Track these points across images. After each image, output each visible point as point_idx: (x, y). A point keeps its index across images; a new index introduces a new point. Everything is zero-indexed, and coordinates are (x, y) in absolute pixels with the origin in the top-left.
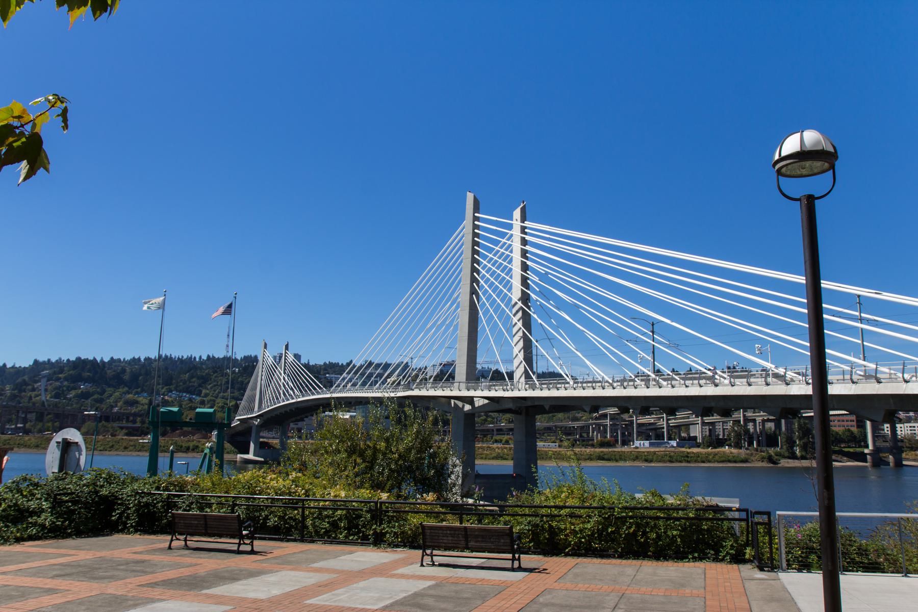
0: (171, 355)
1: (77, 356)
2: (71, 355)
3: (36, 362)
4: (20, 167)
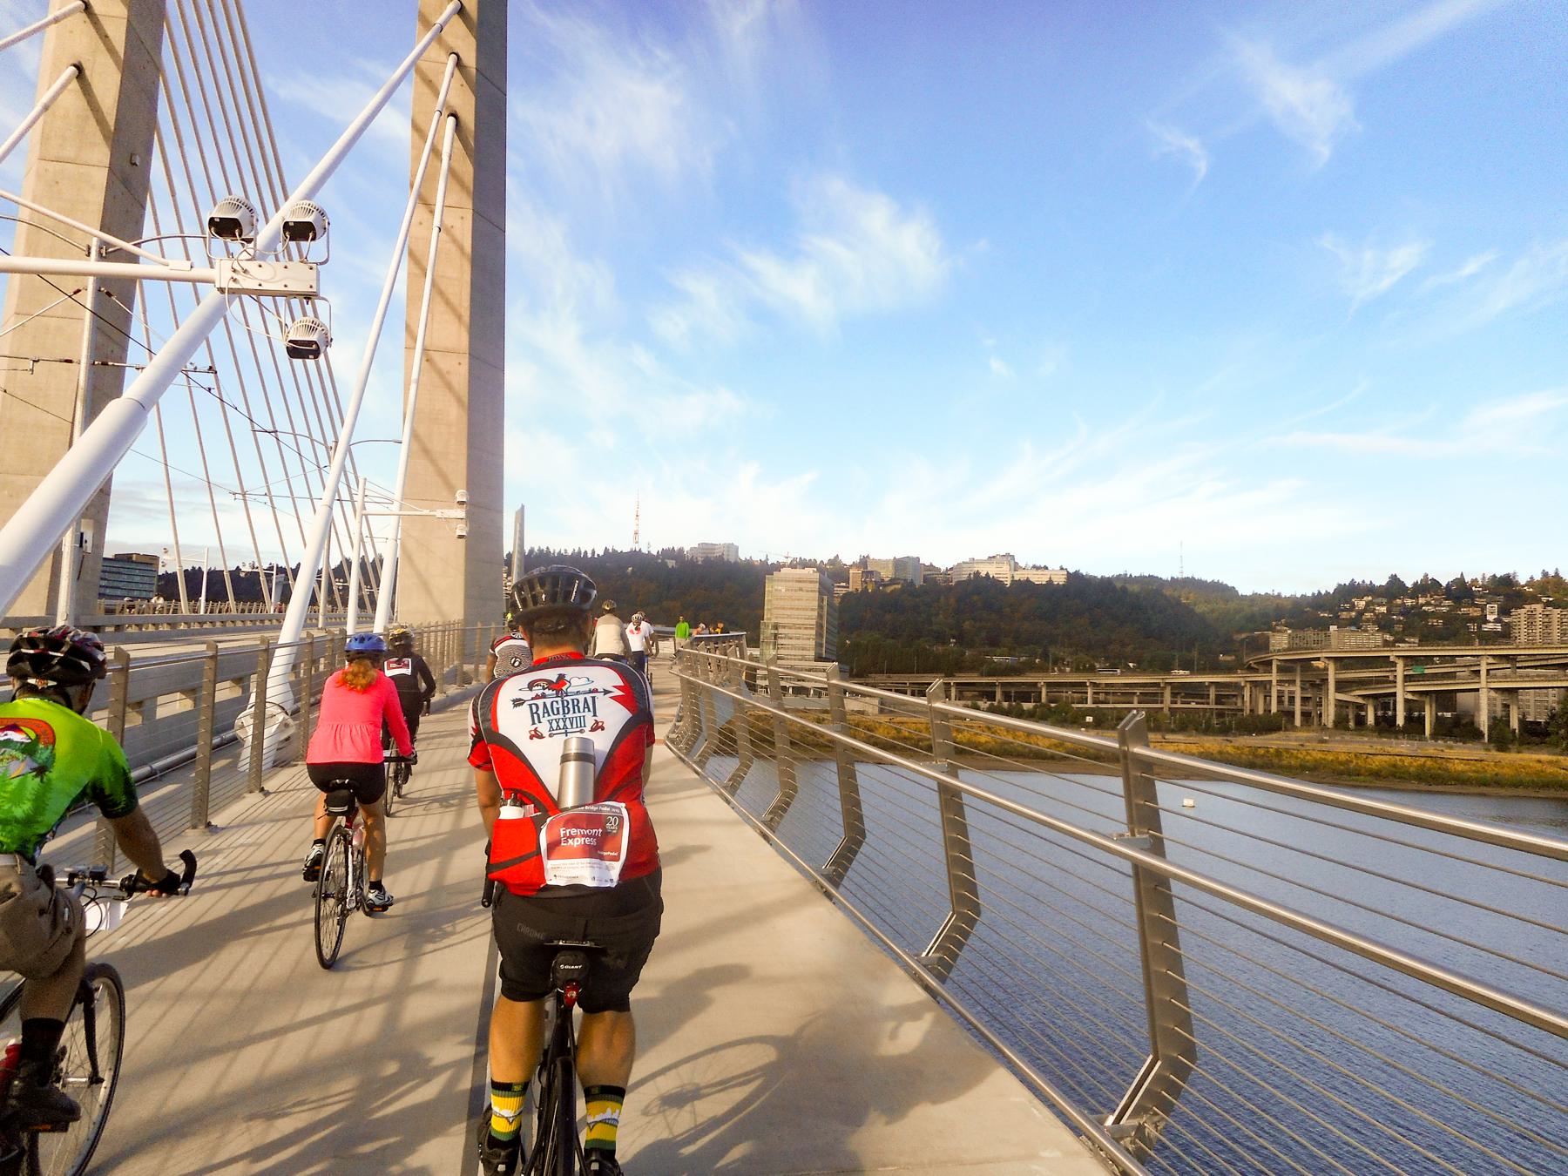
0: (548, 548)
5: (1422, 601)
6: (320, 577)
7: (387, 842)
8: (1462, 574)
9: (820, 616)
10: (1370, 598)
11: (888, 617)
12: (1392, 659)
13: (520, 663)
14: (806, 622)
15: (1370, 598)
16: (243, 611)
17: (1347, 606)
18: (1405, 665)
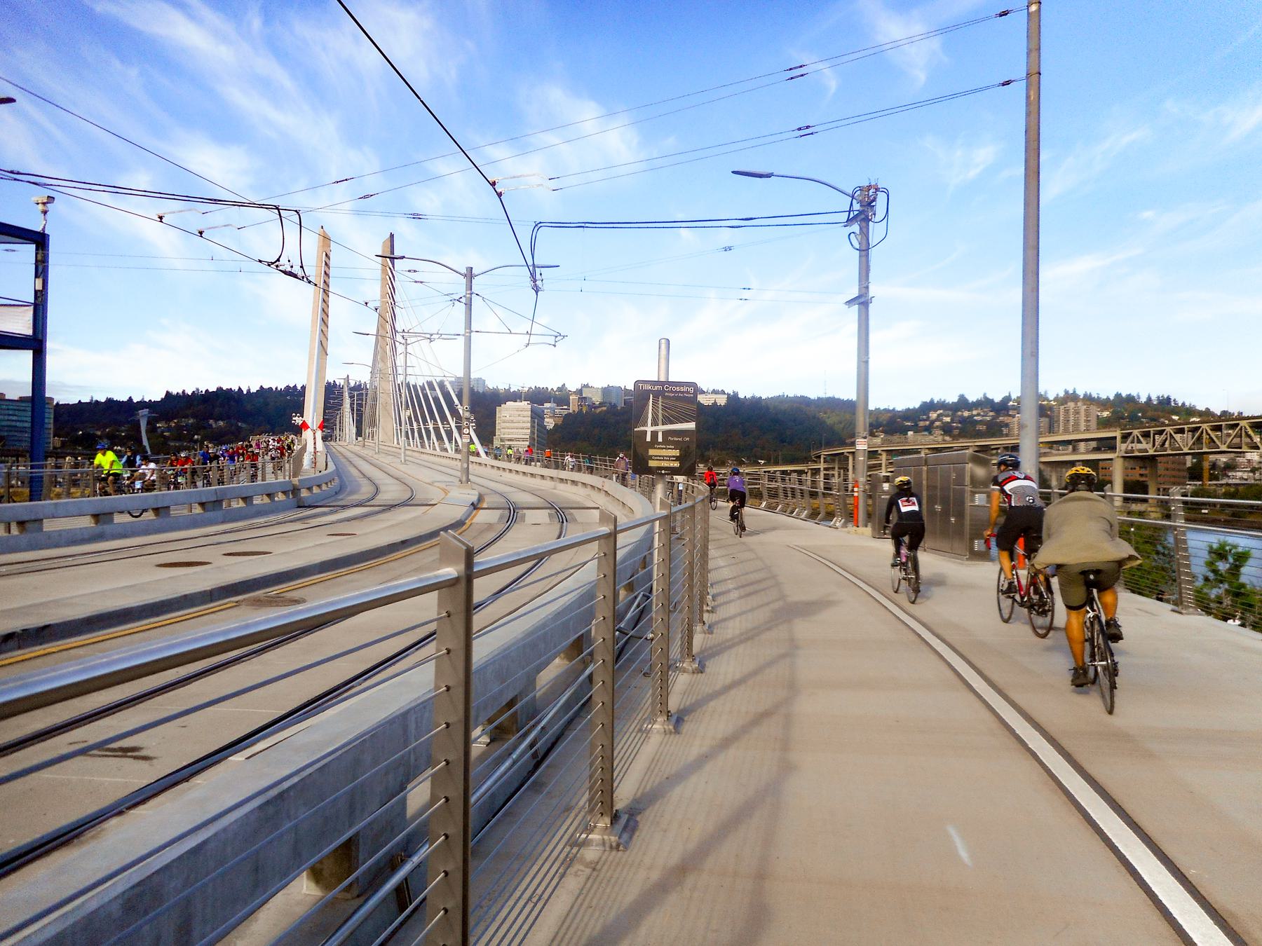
1: (959, 395)
2: (209, 384)
3: (168, 394)
9: (532, 433)
10: (941, 411)
11: (596, 431)
12: (879, 452)
14: (524, 437)
15: (941, 411)
17: (925, 417)
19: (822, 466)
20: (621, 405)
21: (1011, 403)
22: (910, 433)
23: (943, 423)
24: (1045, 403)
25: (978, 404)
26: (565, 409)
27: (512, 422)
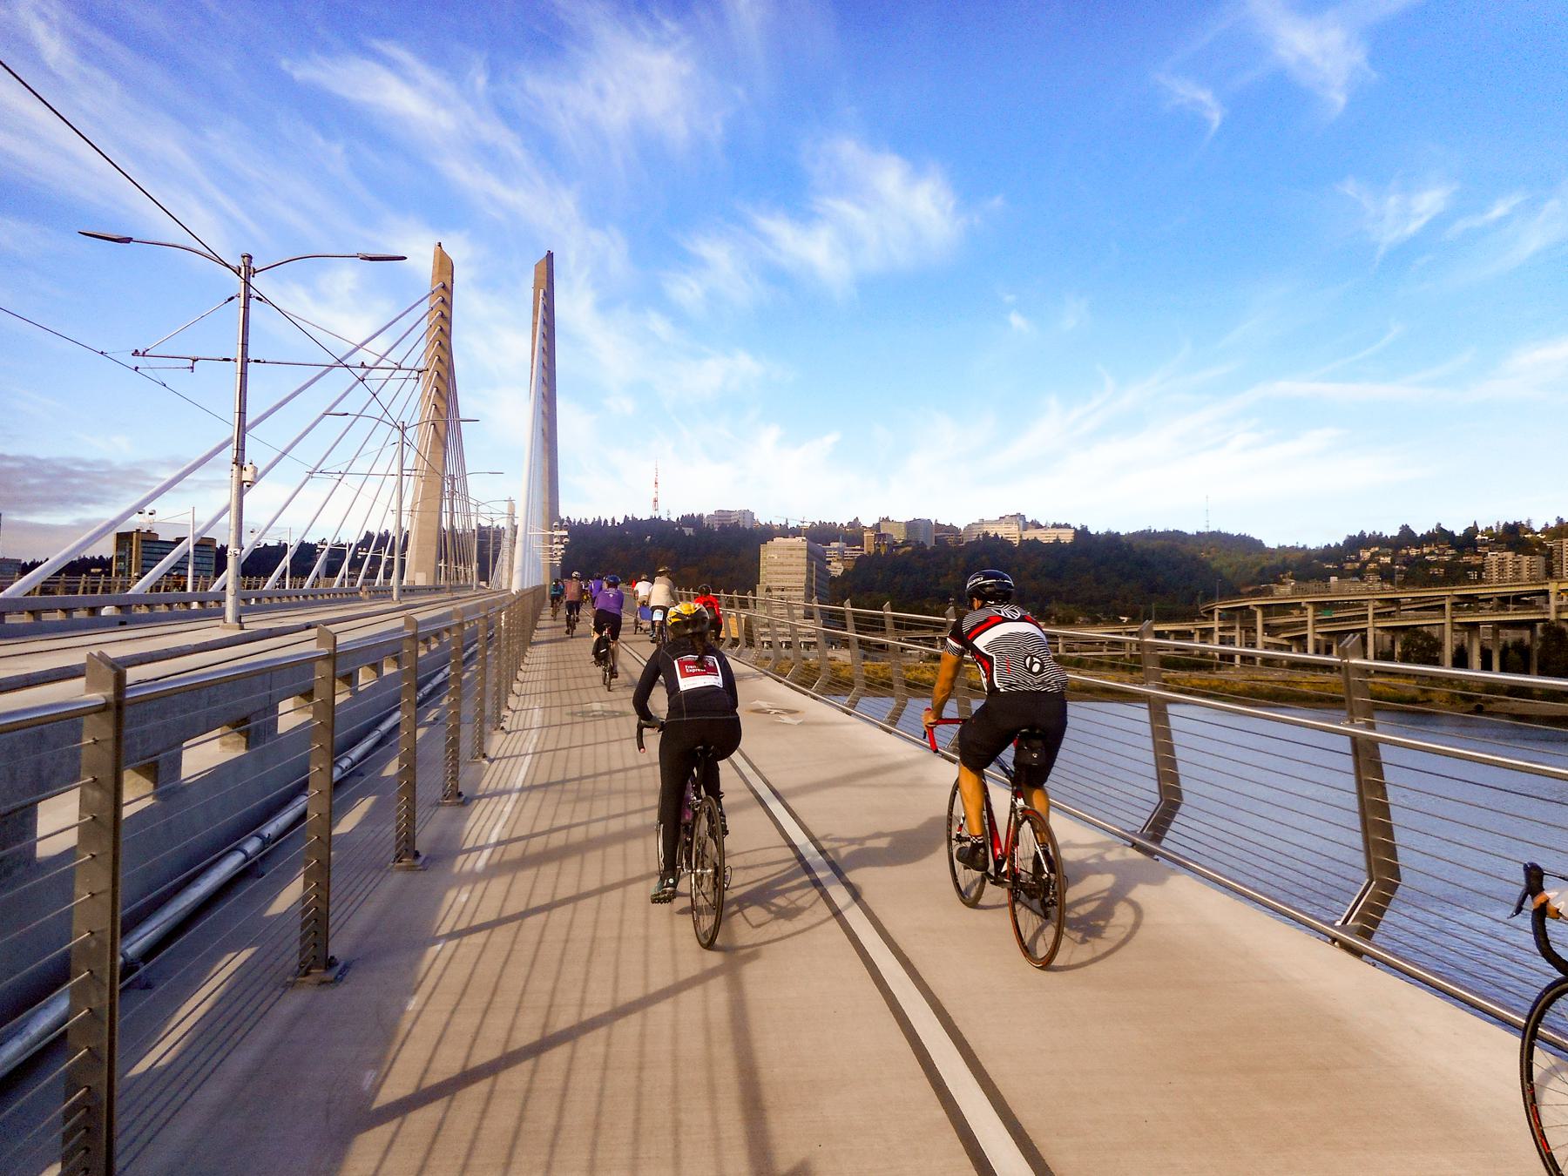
0: (568, 517)
4: (69, 1124)
5: (1426, 550)
6: (405, 556)
7: (821, 899)
8: (1475, 522)
9: (809, 580)
10: (1377, 549)
13: (1042, 666)
15: (1377, 549)
16: (249, 587)
18: (1315, 611)
19: (1216, 624)
20: (930, 544)
21: (1479, 537)
22: (1333, 579)
23: (1379, 564)
24: (1529, 536)
25: (1429, 539)
26: (859, 550)
27: (782, 564)
